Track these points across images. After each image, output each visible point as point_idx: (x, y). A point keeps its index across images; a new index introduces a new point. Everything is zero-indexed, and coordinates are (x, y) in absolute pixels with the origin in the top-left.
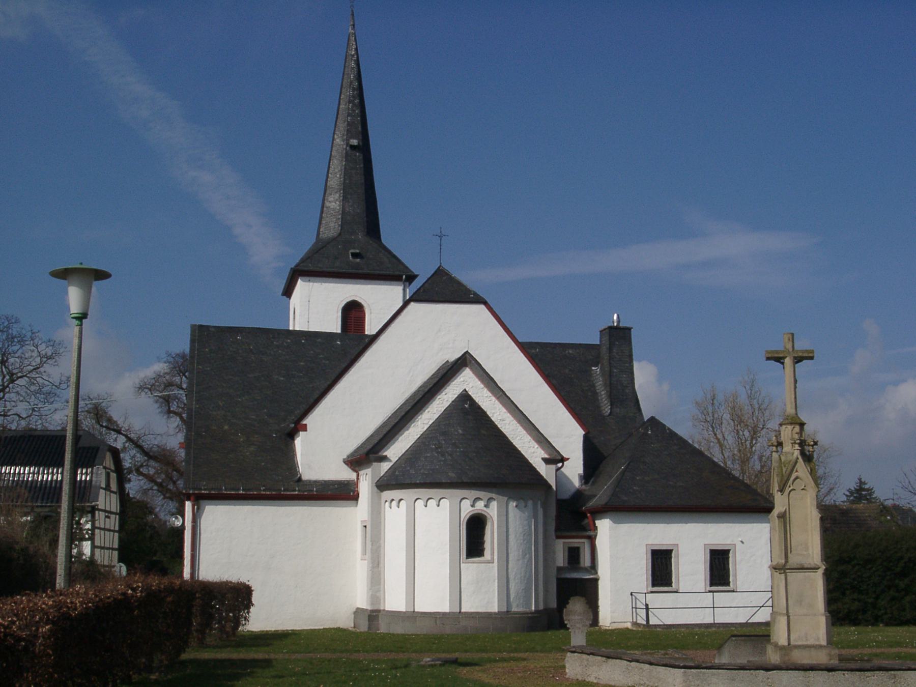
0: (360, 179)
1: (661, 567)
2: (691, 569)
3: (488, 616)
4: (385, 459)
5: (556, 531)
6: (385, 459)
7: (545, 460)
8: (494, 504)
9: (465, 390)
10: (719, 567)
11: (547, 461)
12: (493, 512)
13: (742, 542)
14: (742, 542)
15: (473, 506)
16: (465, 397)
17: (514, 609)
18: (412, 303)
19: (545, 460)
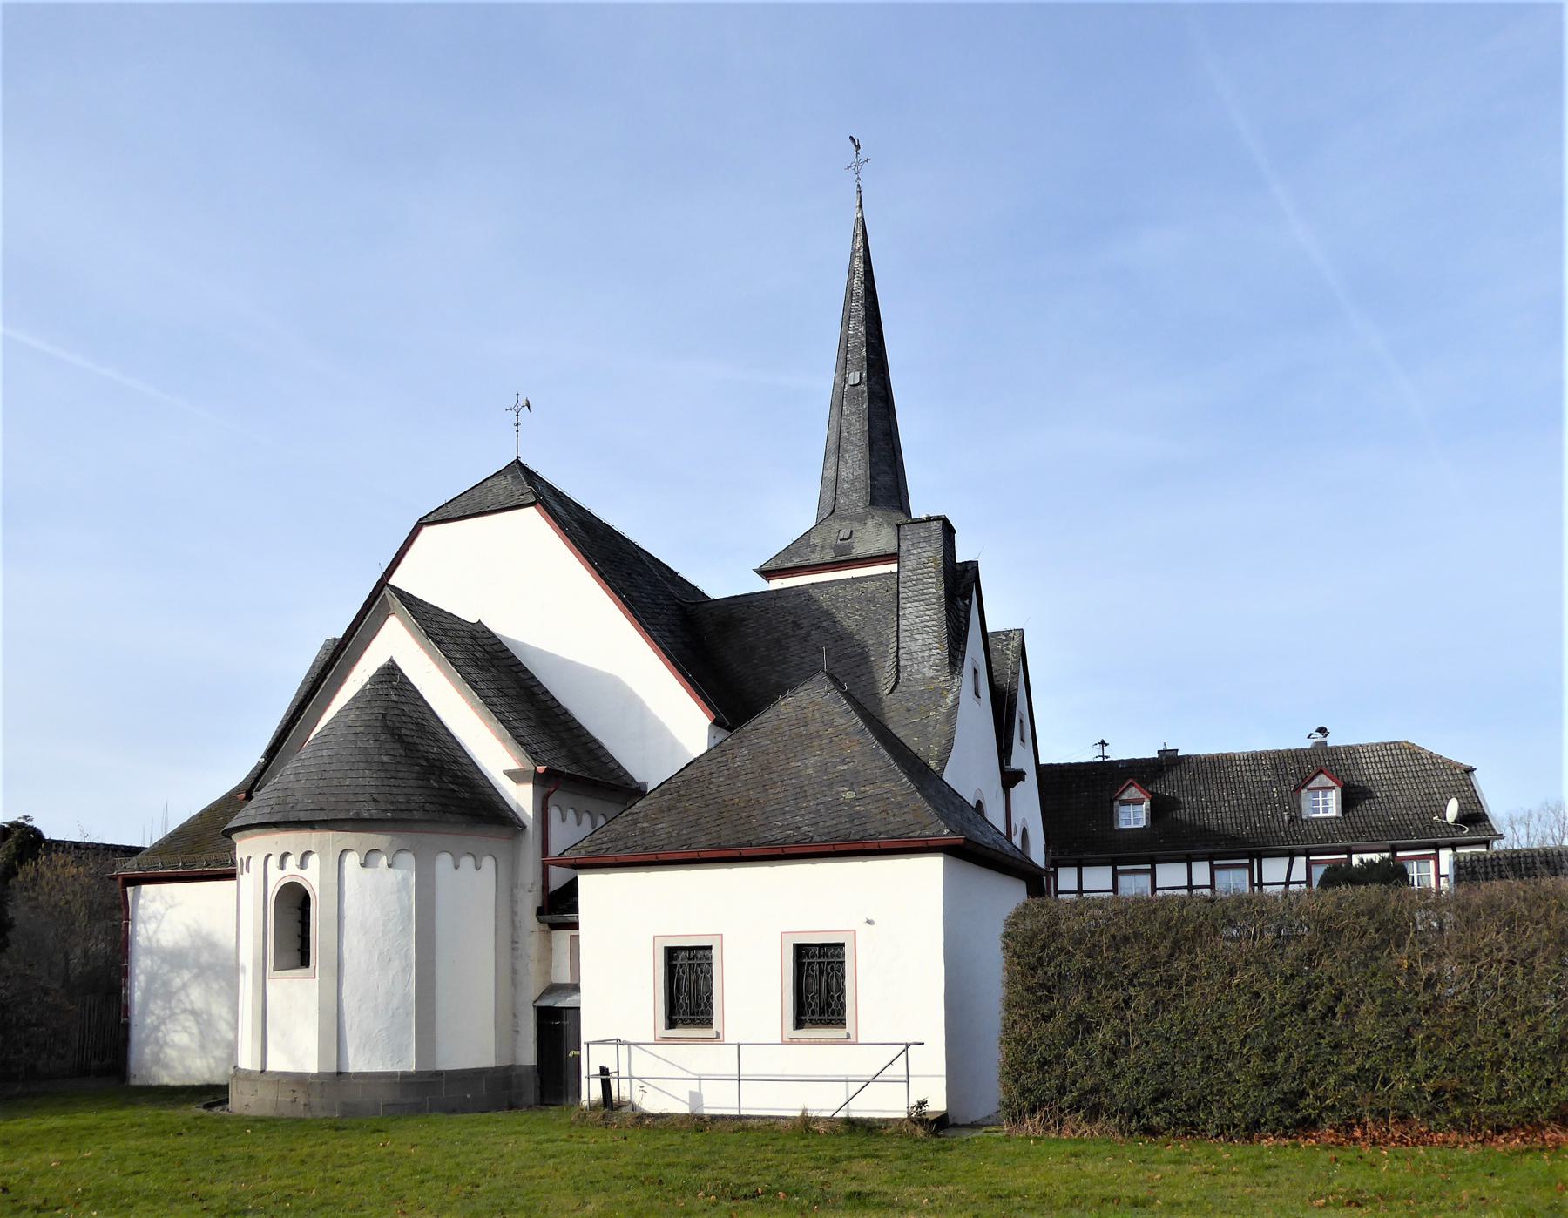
0: (857, 426)
1: (688, 987)
2: (753, 990)
3: (299, 1081)
5: (540, 912)
7: (510, 774)
8: (313, 860)
9: (391, 660)
10: (818, 986)
11: (513, 775)
12: (312, 877)
13: (870, 922)
14: (870, 922)
15: (282, 867)
17: (357, 1063)
18: (426, 531)
19: (510, 774)
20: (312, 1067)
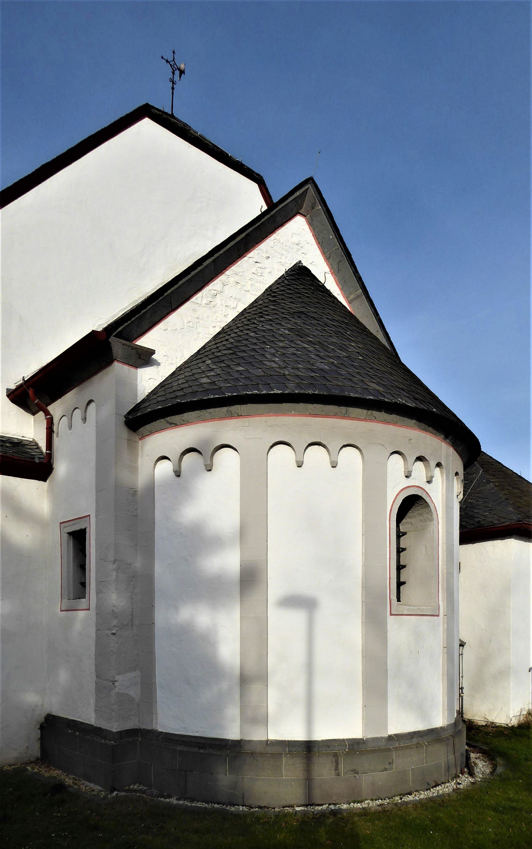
4: (145, 358)
6: (145, 358)
16: (299, 273)
20: (440, 719)
